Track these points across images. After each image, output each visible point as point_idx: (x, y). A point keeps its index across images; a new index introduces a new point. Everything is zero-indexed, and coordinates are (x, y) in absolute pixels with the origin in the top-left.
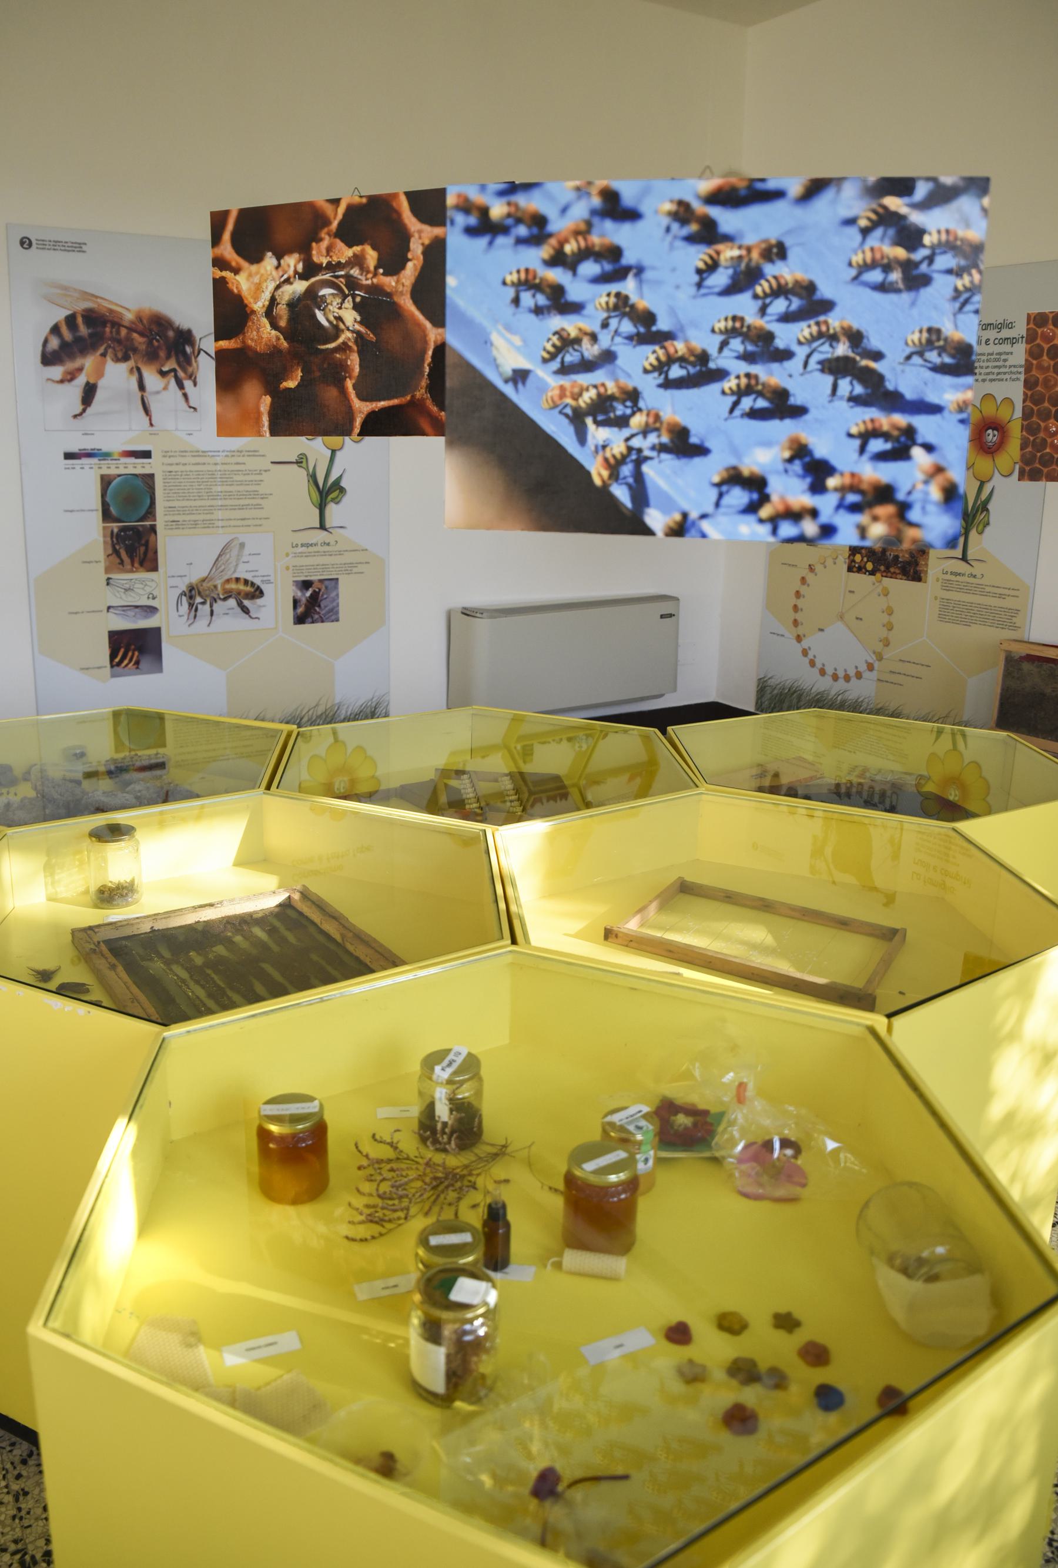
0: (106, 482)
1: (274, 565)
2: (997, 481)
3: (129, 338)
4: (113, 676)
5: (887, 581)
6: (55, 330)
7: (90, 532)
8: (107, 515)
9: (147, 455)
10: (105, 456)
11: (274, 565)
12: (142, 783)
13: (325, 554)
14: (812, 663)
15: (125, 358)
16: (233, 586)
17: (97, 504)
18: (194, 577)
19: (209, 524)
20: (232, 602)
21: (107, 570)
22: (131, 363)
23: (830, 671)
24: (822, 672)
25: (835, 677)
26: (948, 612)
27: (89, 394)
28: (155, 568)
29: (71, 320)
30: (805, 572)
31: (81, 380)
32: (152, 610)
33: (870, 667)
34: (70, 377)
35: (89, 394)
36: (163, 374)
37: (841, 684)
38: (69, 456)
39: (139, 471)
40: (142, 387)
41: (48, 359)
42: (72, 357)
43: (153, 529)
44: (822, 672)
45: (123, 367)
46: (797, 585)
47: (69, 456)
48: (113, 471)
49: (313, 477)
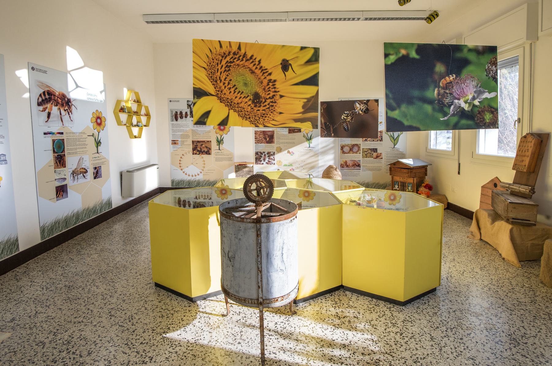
0: (54, 141)
1: (89, 164)
2: (224, 135)
3: (57, 100)
4: (57, 200)
5: (202, 156)
6: (40, 95)
7: (50, 157)
8: (54, 151)
9: (62, 133)
10: (53, 133)
11: (89, 164)
12: (188, 195)
13: (99, 160)
14: (186, 174)
15: (57, 105)
16: (81, 170)
17: (51, 148)
18: (73, 169)
19: (76, 153)
20: (82, 175)
21: (55, 168)
22: (58, 107)
23: (191, 175)
24: (189, 175)
25: (192, 176)
26: (217, 160)
27: (49, 114)
28: (65, 167)
29: (44, 93)
30: (182, 156)
31: (47, 111)
32: (65, 179)
33: (201, 173)
34: (44, 110)
35: (49, 114)
36: (65, 110)
37: (194, 177)
38: (45, 134)
39: (61, 138)
40: (61, 114)
41: (39, 104)
42: (44, 104)
43: (64, 155)
44: (189, 175)
45: (57, 108)
46: (180, 159)
47: (45, 134)
48: (55, 138)
49: (95, 139)
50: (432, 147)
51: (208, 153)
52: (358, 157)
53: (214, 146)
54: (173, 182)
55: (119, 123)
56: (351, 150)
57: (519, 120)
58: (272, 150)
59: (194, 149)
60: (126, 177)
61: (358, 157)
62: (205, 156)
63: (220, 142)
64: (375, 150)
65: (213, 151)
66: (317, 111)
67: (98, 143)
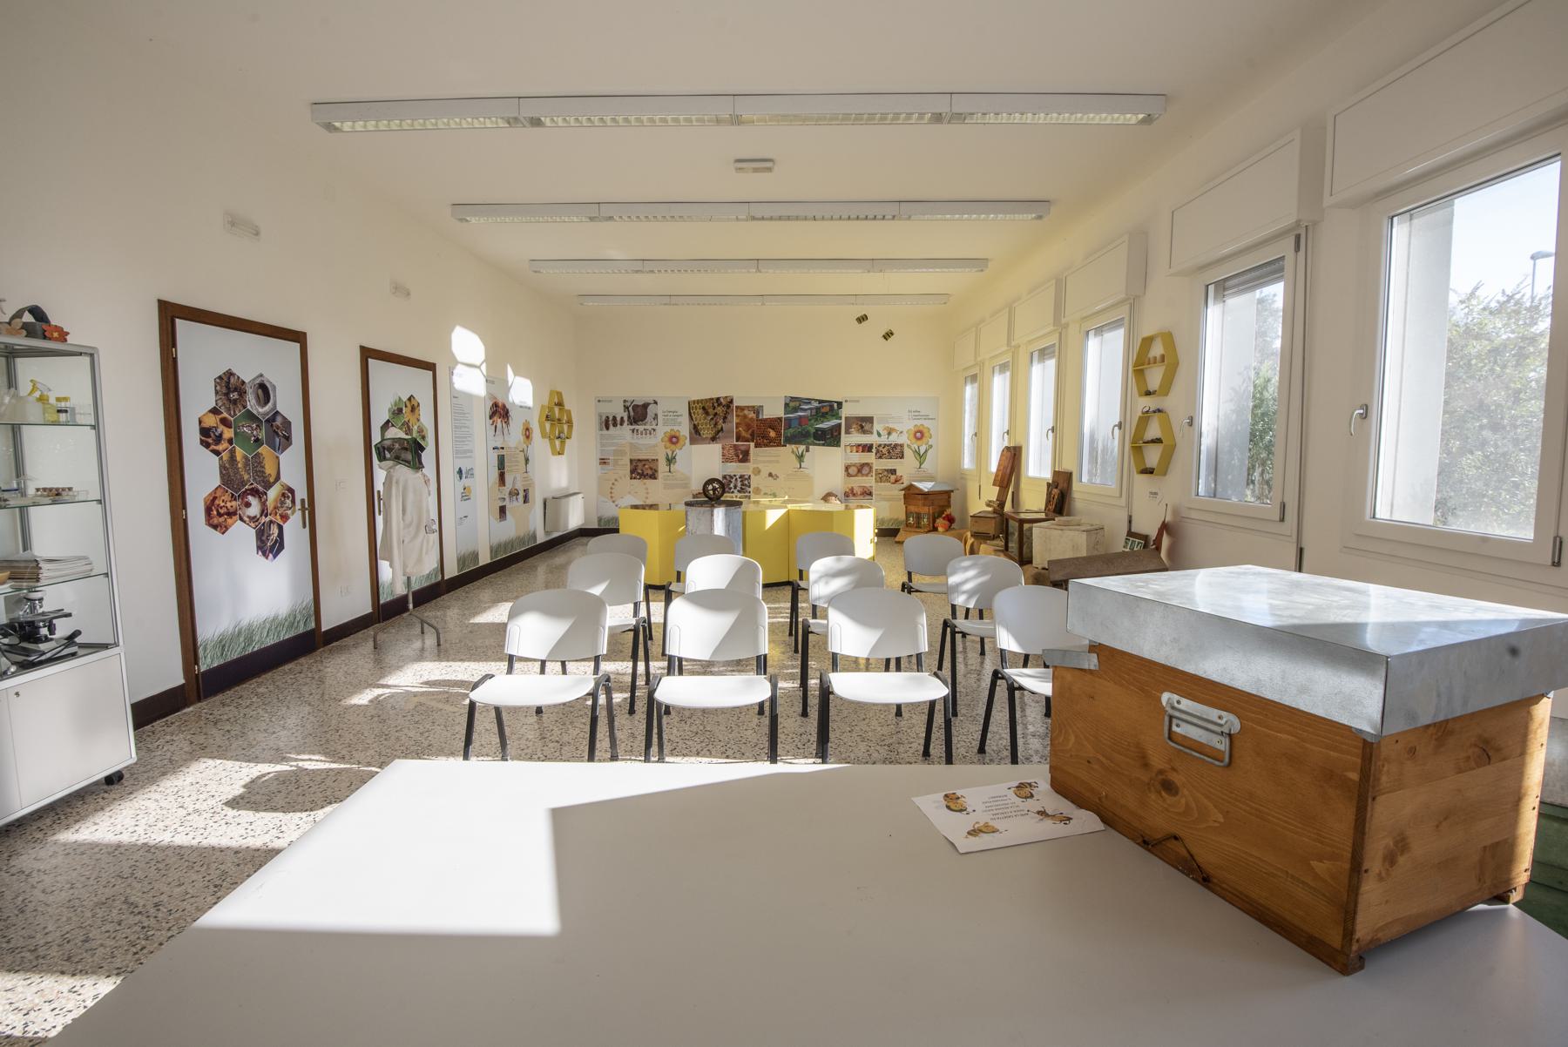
11: (520, 487)
26: (666, 487)
50: (1382, 513)
51: (653, 477)
52: (869, 481)
53: (662, 467)
54: (600, 520)
55: (544, 435)
56: (859, 471)
57: (1120, 426)
58: (746, 473)
59: (632, 472)
60: (553, 505)
61: (869, 481)
62: (649, 482)
63: (670, 461)
64: (893, 472)
65: (660, 475)
66: (771, 624)
67: (527, 460)
